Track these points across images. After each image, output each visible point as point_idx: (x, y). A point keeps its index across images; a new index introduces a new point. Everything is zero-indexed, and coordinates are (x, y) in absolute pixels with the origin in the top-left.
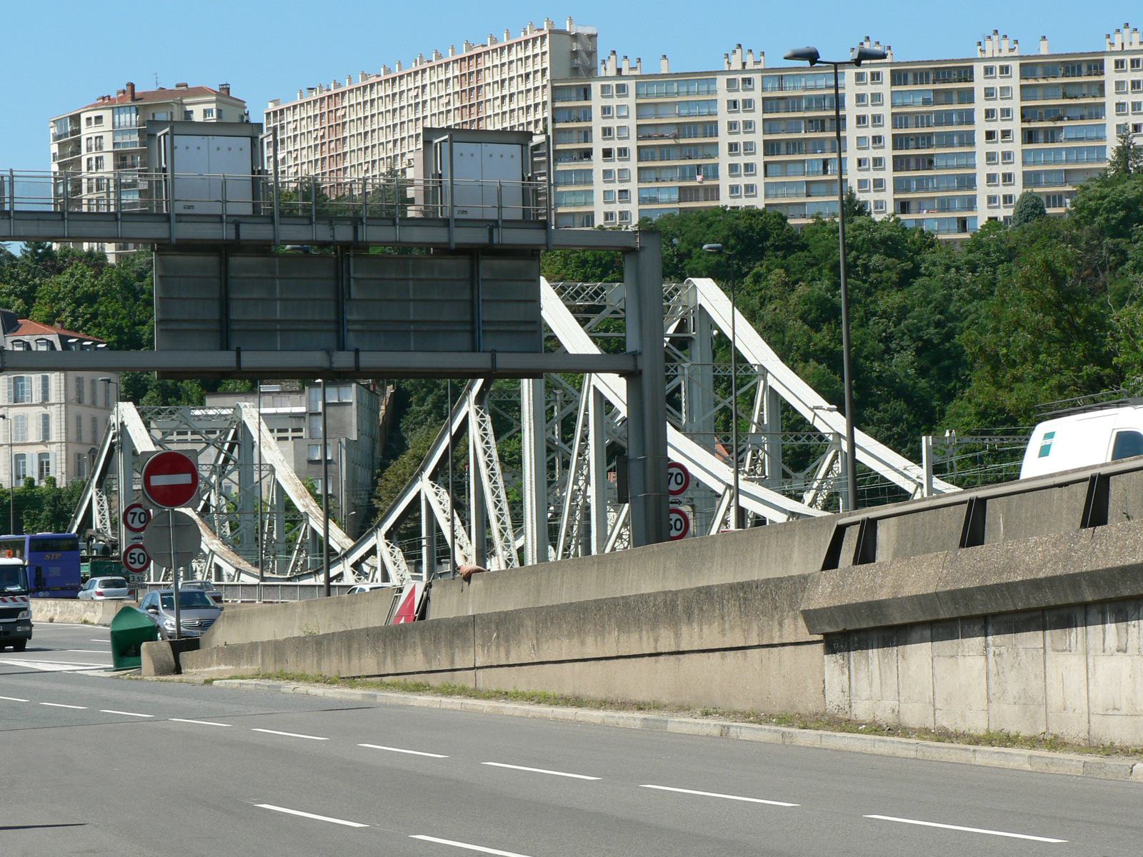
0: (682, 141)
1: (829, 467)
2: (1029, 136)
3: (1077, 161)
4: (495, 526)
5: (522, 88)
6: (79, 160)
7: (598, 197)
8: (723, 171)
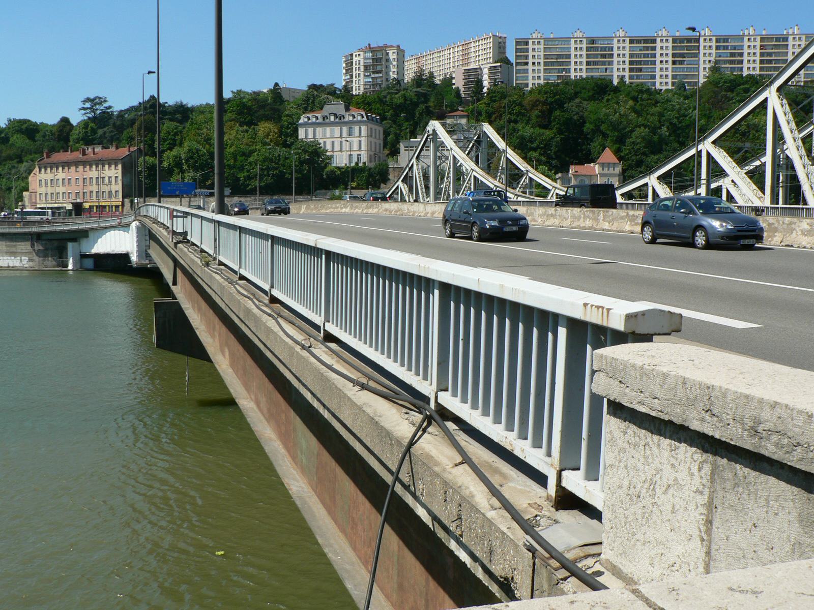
0: (558, 60)
1: (524, 181)
2: (674, 63)
3: (690, 72)
4: (420, 192)
5: (483, 53)
6: (352, 68)
7: (530, 78)
8: (572, 70)
